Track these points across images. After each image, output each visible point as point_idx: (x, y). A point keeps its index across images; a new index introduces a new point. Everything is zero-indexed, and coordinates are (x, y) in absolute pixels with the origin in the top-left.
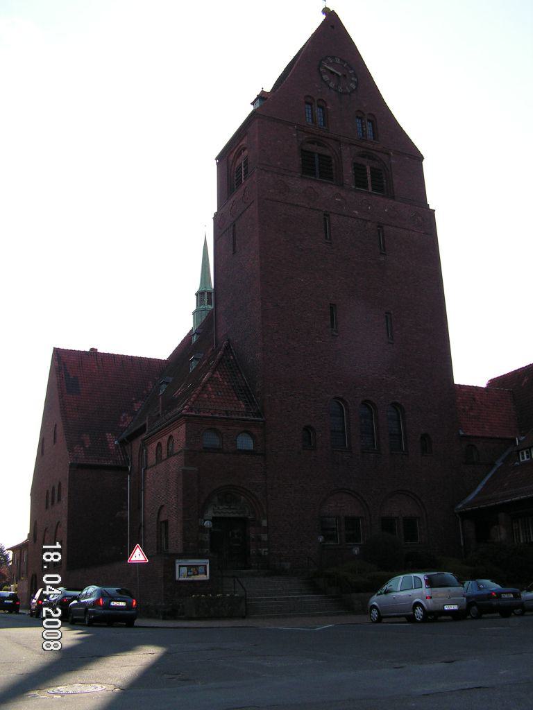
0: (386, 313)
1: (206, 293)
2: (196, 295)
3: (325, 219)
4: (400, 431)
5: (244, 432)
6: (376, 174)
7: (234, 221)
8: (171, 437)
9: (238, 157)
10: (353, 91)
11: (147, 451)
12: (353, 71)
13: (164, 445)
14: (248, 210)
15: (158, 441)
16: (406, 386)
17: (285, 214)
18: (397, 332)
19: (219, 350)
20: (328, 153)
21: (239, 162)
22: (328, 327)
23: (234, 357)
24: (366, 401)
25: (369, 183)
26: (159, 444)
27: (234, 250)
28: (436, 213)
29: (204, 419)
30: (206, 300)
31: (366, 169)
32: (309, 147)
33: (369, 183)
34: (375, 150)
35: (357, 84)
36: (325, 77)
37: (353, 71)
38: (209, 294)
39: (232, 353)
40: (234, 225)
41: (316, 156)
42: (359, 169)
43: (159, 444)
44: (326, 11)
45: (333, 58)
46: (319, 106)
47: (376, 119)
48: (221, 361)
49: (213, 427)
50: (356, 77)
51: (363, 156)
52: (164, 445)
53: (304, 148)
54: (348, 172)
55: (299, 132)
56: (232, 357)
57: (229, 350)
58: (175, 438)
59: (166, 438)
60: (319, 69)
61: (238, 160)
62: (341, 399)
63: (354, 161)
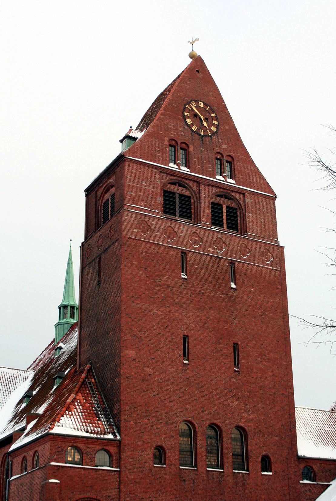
0: (234, 343)
1: (69, 308)
2: (60, 308)
3: (182, 256)
4: (243, 452)
5: (102, 449)
6: (233, 213)
7: (100, 254)
8: (36, 452)
9: (106, 193)
10: (213, 133)
11: (12, 462)
12: (214, 115)
13: (29, 459)
14: (113, 247)
15: (23, 455)
16: (249, 411)
17: (146, 252)
18: (243, 361)
19: (82, 372)
20: (187, 193)
21: (106, 197)
22: (180, 356)
23: (95, 379)
24: (212, 424)
25: (225, 221)
26: (24, 458)
27: (99, 281)
28: (285, 249)
29: (67, 437)
30: (69, 315)
31: (222, 209)
32: (172, 188)
33: (225, 221)
34: (231, 191)
35: (217, 127)
36: (189, 121)
37: (214, 115)
38: (72, 307)
39: (94, 376)
40: (100, 258)
41: (177, 196)
42: (216, 208)
43: (24, 458)
44: (192, 56)
45: (198, 133)
46: (182, 149)
47: (234, 161)
48: (84, 383)
49: (75, 444)
50: (217, 120)
51: (221, 196)
52: (29, 459)
53: (166, 189)
54: (206, 211)
55: (163, 174)
56: (93, 380)
57: (91, 373)
58: (40, 453)
59: (31, 453)
60: (183, 113)
61: (106, 196)
62: (190, 422)
63: (211, 201)
